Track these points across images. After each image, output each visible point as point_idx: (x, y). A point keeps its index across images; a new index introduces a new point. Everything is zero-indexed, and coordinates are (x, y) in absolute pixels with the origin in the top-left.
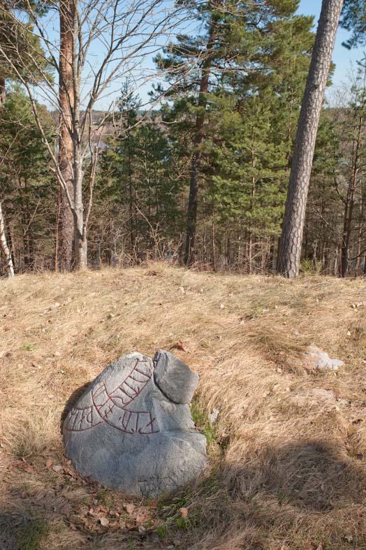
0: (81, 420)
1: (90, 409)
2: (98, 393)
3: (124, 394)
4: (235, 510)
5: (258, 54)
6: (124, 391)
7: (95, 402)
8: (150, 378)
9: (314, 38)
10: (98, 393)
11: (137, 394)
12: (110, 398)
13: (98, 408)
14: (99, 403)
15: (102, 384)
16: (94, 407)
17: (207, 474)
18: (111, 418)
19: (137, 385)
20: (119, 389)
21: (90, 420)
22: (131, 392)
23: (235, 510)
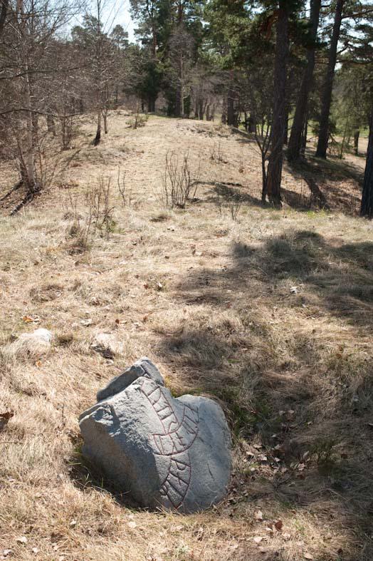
0: (180, 479)
1: (173, 462)
2: (160, 445)
3: (168, 418)
4: (81, 104)
5: (82, 114)
6: (165, 417)
7: (168, 453)
8: (159, 387)
9: (359, 204)
10: (160, 445)
11: (169, 406)
12: (169, 433)
13: (175, 451)
14: (171, 447)
15: (152, 437)
16: (173, 456)
17: (258, 20)
18: (187, 442)
19: (161, 400)
20: (163, 421)
21: (184, 466)
22: (167, 411)
23: (81, 104)
